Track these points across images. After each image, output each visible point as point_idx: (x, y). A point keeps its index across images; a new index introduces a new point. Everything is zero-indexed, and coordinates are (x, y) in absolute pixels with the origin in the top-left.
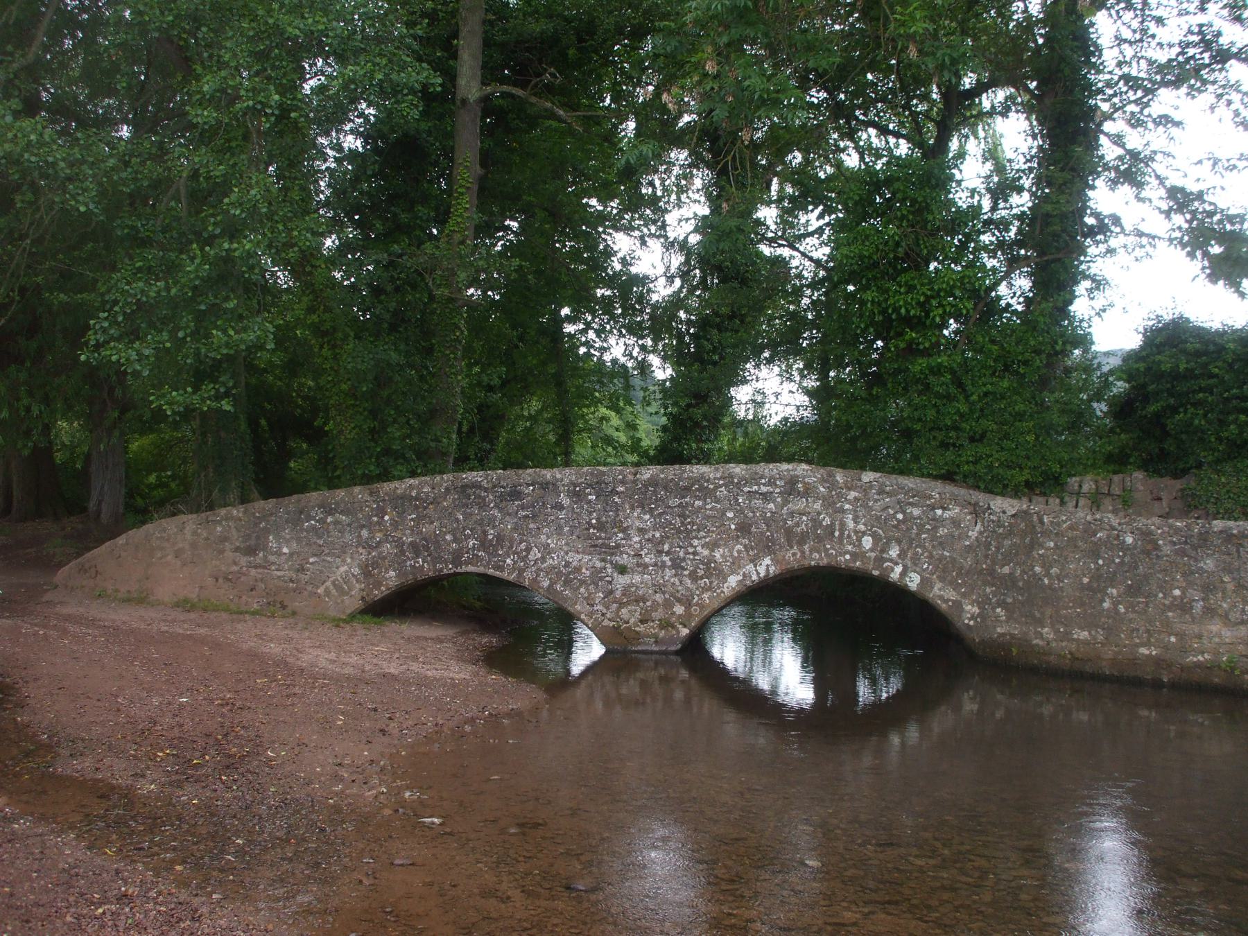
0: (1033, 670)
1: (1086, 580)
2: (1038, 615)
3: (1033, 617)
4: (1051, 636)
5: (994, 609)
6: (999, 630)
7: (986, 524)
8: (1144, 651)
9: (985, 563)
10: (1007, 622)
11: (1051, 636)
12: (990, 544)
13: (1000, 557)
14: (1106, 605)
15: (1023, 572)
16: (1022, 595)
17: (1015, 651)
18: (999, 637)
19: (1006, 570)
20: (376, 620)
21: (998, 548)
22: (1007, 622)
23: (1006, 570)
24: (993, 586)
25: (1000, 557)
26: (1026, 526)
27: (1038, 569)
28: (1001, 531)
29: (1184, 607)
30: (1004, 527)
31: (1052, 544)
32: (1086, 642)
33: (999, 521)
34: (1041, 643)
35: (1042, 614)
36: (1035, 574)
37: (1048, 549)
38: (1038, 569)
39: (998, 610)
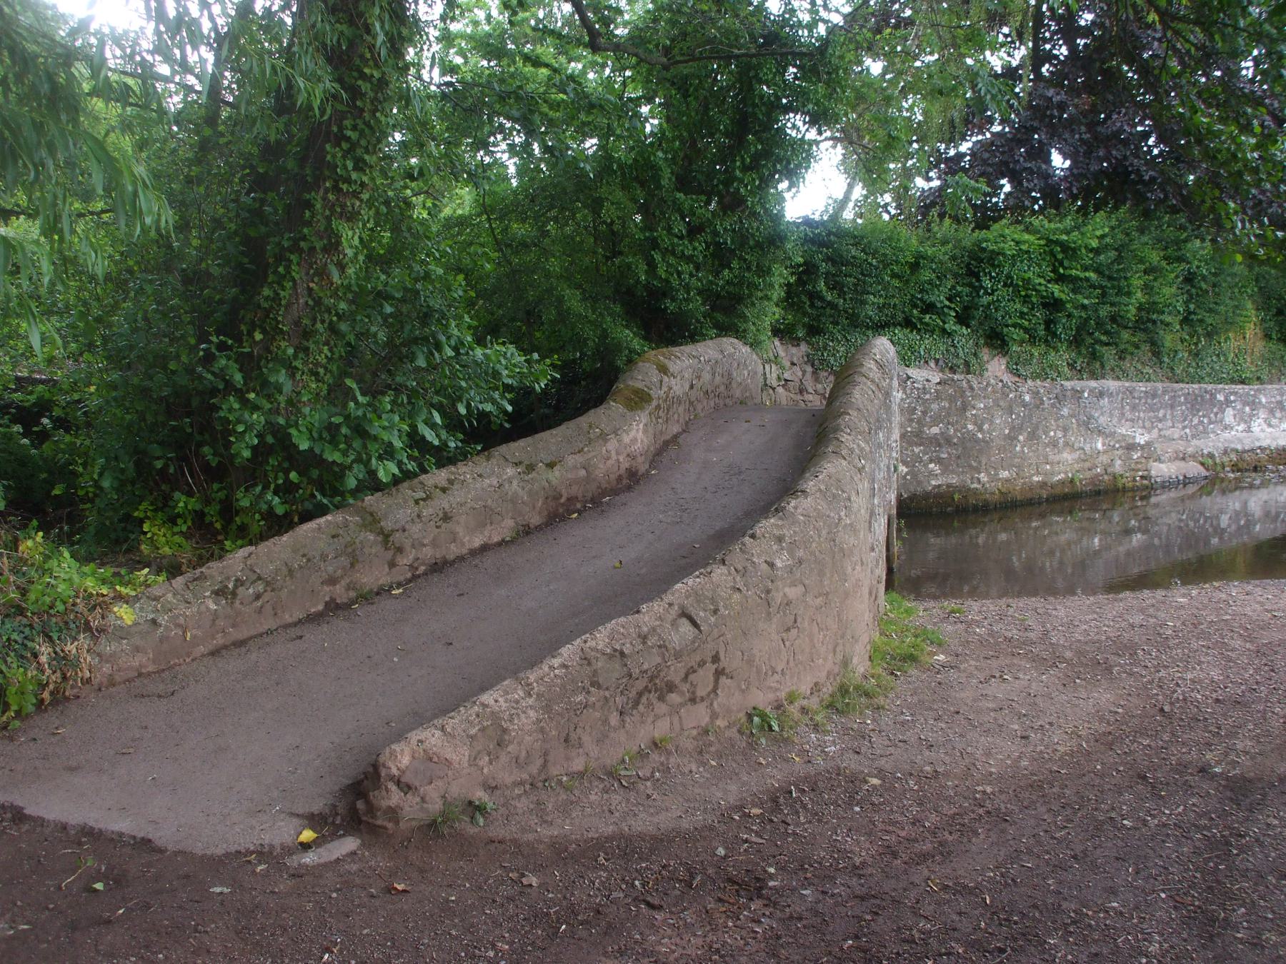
0: (976, 509)
1: (1007, 431)
2: (974, 464)
3: (970, 466)
4: (986, 479)
5: (926, 466)
6: (933, 483)
7: (908, 392)
8: (1036, 479)
9: (910, 426)
10: (942, 474)
11: (986, 479)
12: (915, 409)
13: (928, 419)
14: (1018, 449)
15: (956, 430)
16: (957, 450)
17: (956, 497)
18: (933, 489)
19: (935, 430)
20: (1029, 496)
21: (924, 413)
22: (942, 474)
23: (935, 430)
24: (920, 445)
25: (928, 419)
26: (955, 391)
27: (970, 427)
28: (927, 396)
29: (1054, 444)
30: (931, 394)
31: (982, 406)
32: (1007, 480)
33: (924, 388)
34: (978, 486)
35: (980, 462)
36: (968, 432)
37: (980, 409)
38: (970, 427)
39: (932, 466)
